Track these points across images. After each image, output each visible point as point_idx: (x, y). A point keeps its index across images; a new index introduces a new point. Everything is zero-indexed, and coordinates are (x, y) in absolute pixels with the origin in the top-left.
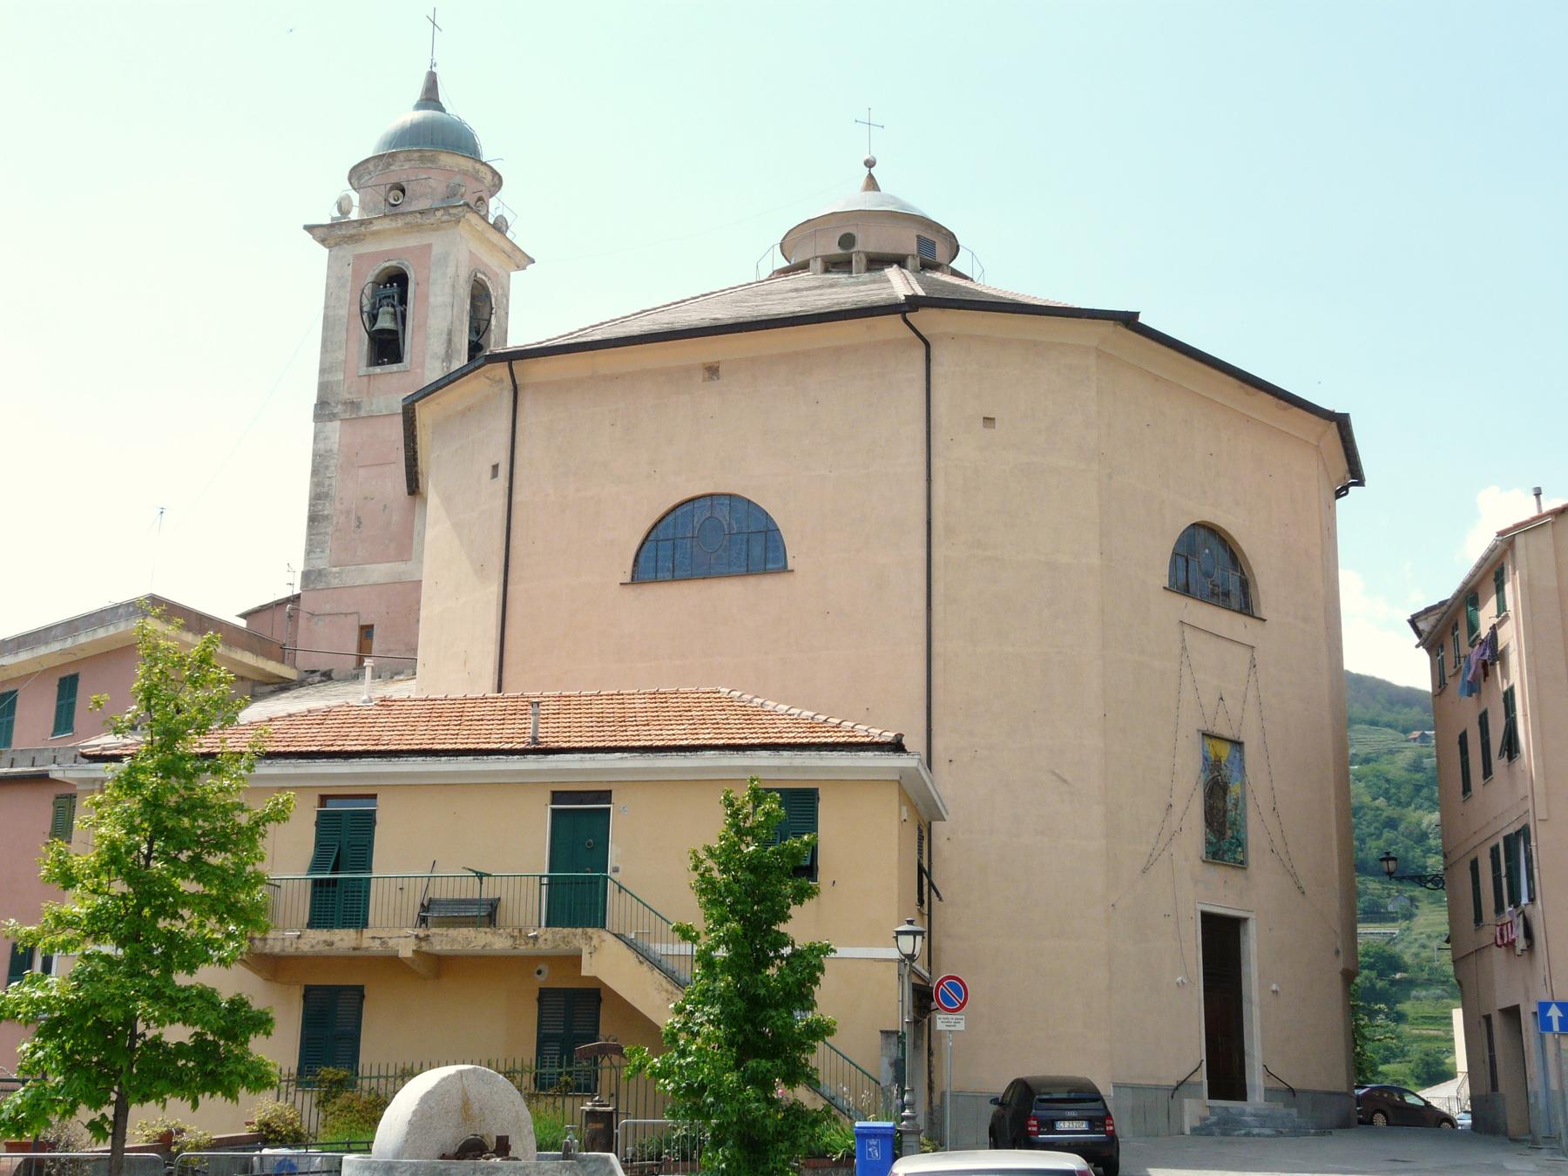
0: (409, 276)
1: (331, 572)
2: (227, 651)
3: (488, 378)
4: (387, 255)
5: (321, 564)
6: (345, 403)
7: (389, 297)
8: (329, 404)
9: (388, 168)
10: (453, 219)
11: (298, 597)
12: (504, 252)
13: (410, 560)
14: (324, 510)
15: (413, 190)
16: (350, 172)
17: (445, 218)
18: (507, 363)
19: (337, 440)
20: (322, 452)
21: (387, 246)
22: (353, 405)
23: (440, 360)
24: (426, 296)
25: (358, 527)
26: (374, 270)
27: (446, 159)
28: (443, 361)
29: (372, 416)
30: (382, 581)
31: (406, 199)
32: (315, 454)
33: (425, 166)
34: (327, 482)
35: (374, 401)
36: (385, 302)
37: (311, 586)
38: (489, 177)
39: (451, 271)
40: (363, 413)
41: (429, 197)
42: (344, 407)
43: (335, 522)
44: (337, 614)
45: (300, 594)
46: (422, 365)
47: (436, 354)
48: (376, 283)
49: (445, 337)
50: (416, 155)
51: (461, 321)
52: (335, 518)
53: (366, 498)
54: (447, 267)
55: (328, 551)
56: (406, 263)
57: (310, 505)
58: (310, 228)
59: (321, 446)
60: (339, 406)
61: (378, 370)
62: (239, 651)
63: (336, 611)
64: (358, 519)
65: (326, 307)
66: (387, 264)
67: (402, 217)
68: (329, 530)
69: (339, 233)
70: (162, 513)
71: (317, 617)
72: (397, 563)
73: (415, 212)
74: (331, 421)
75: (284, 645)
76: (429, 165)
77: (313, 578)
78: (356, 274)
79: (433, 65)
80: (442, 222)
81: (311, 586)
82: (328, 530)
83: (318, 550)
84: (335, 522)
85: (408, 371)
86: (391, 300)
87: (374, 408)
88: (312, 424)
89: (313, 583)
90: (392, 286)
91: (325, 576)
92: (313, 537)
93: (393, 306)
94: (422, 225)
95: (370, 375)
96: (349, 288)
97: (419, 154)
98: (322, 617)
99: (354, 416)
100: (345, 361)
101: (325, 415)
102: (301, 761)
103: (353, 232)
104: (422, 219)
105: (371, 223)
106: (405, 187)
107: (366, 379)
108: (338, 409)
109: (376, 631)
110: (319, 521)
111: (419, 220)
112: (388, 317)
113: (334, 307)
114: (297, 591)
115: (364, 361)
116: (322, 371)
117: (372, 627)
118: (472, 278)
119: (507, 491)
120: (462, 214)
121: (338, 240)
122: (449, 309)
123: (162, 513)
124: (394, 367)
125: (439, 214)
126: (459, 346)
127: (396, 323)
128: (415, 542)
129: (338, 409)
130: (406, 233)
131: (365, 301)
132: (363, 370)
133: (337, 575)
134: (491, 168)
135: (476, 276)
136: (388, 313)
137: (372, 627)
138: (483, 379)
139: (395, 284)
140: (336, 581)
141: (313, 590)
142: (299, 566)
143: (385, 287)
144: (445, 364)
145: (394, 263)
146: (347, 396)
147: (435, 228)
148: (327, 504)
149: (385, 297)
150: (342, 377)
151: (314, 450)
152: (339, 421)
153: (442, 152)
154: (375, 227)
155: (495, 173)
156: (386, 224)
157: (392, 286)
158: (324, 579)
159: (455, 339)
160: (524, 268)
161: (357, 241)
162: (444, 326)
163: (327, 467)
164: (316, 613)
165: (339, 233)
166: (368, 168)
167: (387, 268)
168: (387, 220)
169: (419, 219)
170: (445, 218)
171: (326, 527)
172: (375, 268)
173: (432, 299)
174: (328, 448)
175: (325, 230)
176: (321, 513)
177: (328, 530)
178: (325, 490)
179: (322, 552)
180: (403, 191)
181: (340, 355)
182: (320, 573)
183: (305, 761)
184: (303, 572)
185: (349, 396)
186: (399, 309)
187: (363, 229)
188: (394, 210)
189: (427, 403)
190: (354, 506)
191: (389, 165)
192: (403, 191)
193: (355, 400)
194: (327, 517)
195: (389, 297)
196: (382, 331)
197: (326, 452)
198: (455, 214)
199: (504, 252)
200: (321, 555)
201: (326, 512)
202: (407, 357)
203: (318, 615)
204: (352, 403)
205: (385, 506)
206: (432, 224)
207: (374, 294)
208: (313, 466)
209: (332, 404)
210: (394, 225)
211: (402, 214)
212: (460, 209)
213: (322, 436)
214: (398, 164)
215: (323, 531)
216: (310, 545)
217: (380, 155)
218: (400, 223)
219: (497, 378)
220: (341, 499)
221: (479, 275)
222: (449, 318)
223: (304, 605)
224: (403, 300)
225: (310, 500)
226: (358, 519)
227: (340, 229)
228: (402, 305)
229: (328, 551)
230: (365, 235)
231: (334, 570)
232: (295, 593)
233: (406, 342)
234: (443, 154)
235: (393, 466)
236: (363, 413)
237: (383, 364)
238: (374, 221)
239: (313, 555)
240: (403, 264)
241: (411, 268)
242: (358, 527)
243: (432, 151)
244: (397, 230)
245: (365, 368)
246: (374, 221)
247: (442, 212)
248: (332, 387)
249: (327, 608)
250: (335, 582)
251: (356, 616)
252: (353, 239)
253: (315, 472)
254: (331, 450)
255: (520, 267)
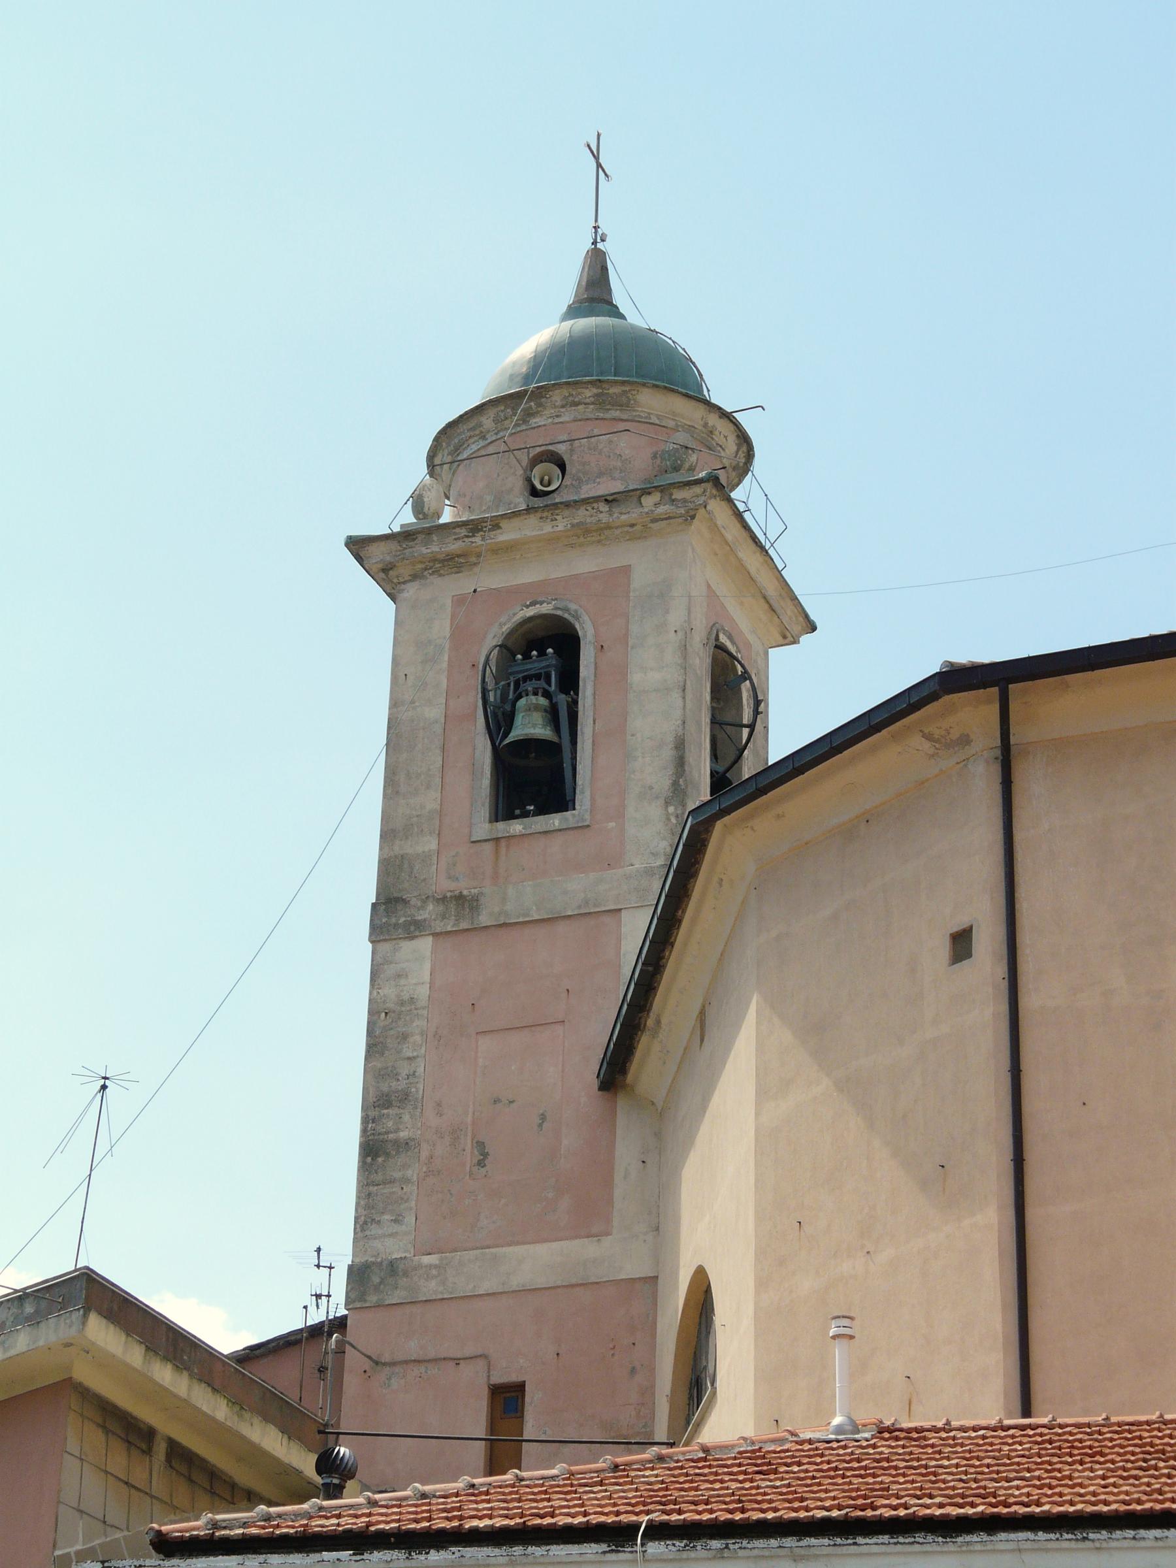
0: (580, 634)
1: (420, 1266)
2: (236, 1418)
3: (929, 737)
4: (532, 593)
5: (393, 1248)
6: (443, 899)
7: (538, 677)
8: (405, 902)
9: (525, 422)
10: (682, 511)
11: (339, 1324)
12: (765, 598)
13: (608, 1234)
14: (397, 1130)
15: (584, 464)
16: (437, 439)
17: (663, 509)
18: (995, 691)
19: (427, 977)
20: (390, 1005)
21: (528, 575)
22: (464, 903)
23: (661, 801)
24: (622, 671)
25: (481, 1164)
26: (501, 625)
27: (650, 402)
28: (667, 803)
29: (504, 925)
30: (541, 1282)
31: (568, 481)
32: (374, 1011)
33: (608, 416)
34: (404, 1069)
35: (511, 891)
36: (529, 686)
37: (373, 1299)
38: (731, 445)
39: (676, 618)
40: (484, 919)
41: (617, 474)
42: (441, 908)
43: (424, 1154)
44: (436, 1360)
45: (345, 1317)
46: (620, 814)
47: (651, 788)
48: (507, 649)
49: (668, 753)
50: (588, 393)
51: (699, 723)
52: (424, 1146)
53: (497, 1101)
54: (667, 612)
55: (410, 1219)
56: (573, 606)
57: (365, 1120)
58: (358, 546)
59: (389, 991)
60: (431, 907)
61: (516, 827)
62: (257, 1420)
63: (432, 1354)
64: (481, 1145)
65: (394, 704)
66: (531, 612)
67: (566, 512)
68: (412, 1173)
69: (424, 550)
70: (104, 1087)
71: (387, 1369)
72: (577, 1242)
73: (597, 499)
74: (412, 938)
75: (326, 1425)
76: (617, 414)
77: (376, 1280)
78: (460, 635)
79: (598, 236)
80: (655, 520)
81: (373, 1299)
82: (409, 1173)
83: (387, 1217)
84: (424, 1154)
85: (588, 826)
86: (542, 683)
87: (509, 907)
88: (369, 946)
89: (377, 1289)
90: (542, 653)
91: (406, 1274)
92: (373, 1189)
93: (547, 695)
94: (608, 527)
95: (497, 839)
96: (445, 665)
97: (595, 391)
98: (397, 1369)
99: (464, 925)
100: (441, 813)
101: (396, 925)
102: (813, 1541)
103: (454, 547)
104: (610, 513)
105: (496, 527)
106: (565, 458)
107: (488, 848)
108: (429, 912)
109: (533, 1399)
110: (387, 1155)
111: (604, 518)
112: (538, 717)
113: (413, 702)
114: (337, 1306)
115: (484, 810)
116: (388, 835)
117: (520, 1388)
118: (713, 642)
119: (1005, 985)
120: (701, 500)
121: (420, 566)
122: (676, 696)
123: (104, 1087)
124: (555, 820)
125: (649, 501)
126: (696, 775)
127: (557, 729)
128: (618, 1193)
129: (429, 912)
130: (572, 546)
131: (491, 684)
132: (483, 828)
133: (434, 1272)
134: (737, 425)
135: (717, 638)
136: (537, 708)
137: (520, 1388)
138: (917, 742)
139: (550, 650)
140: (433, 1284)
141: (378, 1306)
142: (342, 1253)
143: (527, 656)
144: (671, 809)
145: (545, 609)
146: (445, 885)
147: (637, 533)
148: (406, 1118)
149: (525, 679)
150: (434, 845)
151: (371, 1001)
152: (430, 938)
153: (644, 385)
154: (508, 534)
155: (744, 440)
156: (531, 528)
157: (542, 653)
158: (403, 1281)
159: (690, 758)
160: (795, 641)
161: (459, 569)
162: (668, 729)
163: (404, 1037)
164: (386, 1358)
165: (424, 550)
166: (480, 425)
167: (531, 619)
168: (533, 520)
169: (603, 514)
170: (663, 509)
171: (405, 1166)
172: (503, 620)
173: (636, 677)
174: (406, 997)
175: (393, 546)
176: (391, 1136)
177: (409, 1173)
178: (402, 1085)
179: (396, 1221)
180: (562, 467)
181: (430, 800)
182: (393, 1268)
183: (826, 1541)
184: (351, 1268)
185: (452, 885)
186: (562, 699)
187: (477, 540)
188: (538, 502)
189: (751, 816)
190: (469, 1119)
191: (529, 414)
192: (562, 467)
193: (465, 892)
194: (406, 1146)
195: (538, 677)
196: (528, 745)
197: (402, 1003)
198: (685, 501)
199: (765, 598)
200: (396, 1228)
201: (403, 1135)
202: (583, 799)
203: (393, 1364)
204: (460, 898)
205: (543, 1117)
206: (632, 525)
207: (503, 672)
208: (370, 1032)
209: (413, 902)
210: (548, 528)
211: (567, 505)
212: (697, 490)
213: (390, 970)
214: (547, 412)
215: (397, 1175)
216: (368, 1207)
217: (511, 395)
218: (562, 524)
219: (955, 734)
220: (439, 1105)
221: (723, 639)
222: (678, 713)
223: (353, 1333)
224: (570, 680)
225: (365, 1108)
226: (481, 1145)
227: (426, 544)
228: (567, 693)
229: (410, 1219)
230: (479, 555)
231: (427, 1260)
232: (338, 1315)
233: (579, 768)
234: (645, 390)
235: (559, 1029)
236: (484, 919)
237: (525, 815)
238: (503, 524)
239: (374, 1230)
240: (567, 610)
241: (586, 618)
242: (481, 1164)
243: (623, 383)
244: (552, 541)
245: (487, 826)
246: (503, 524)
247: (656, 497)
248: (411, 868)
249: (412, 1348)
250: (430, 1288)
251: (481, 1364)
252: (453, 563)
253: (375, 1047)
254: (412, 1000)
255: (789, 638)
